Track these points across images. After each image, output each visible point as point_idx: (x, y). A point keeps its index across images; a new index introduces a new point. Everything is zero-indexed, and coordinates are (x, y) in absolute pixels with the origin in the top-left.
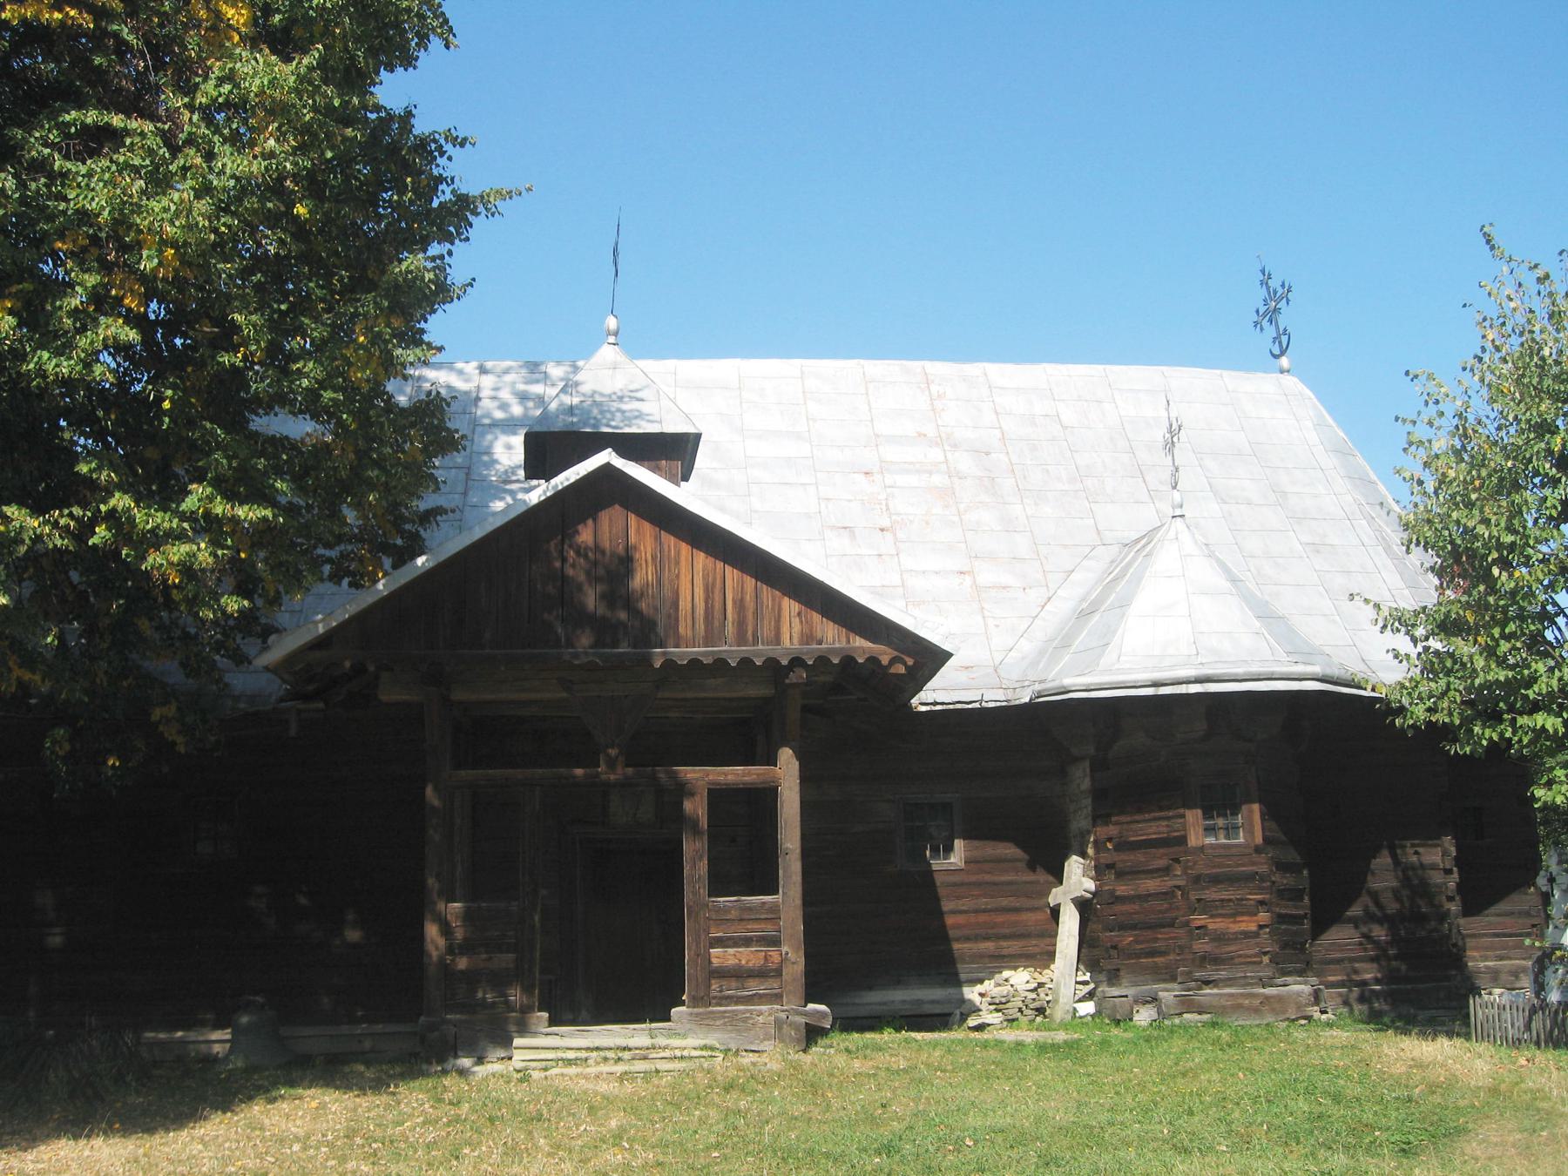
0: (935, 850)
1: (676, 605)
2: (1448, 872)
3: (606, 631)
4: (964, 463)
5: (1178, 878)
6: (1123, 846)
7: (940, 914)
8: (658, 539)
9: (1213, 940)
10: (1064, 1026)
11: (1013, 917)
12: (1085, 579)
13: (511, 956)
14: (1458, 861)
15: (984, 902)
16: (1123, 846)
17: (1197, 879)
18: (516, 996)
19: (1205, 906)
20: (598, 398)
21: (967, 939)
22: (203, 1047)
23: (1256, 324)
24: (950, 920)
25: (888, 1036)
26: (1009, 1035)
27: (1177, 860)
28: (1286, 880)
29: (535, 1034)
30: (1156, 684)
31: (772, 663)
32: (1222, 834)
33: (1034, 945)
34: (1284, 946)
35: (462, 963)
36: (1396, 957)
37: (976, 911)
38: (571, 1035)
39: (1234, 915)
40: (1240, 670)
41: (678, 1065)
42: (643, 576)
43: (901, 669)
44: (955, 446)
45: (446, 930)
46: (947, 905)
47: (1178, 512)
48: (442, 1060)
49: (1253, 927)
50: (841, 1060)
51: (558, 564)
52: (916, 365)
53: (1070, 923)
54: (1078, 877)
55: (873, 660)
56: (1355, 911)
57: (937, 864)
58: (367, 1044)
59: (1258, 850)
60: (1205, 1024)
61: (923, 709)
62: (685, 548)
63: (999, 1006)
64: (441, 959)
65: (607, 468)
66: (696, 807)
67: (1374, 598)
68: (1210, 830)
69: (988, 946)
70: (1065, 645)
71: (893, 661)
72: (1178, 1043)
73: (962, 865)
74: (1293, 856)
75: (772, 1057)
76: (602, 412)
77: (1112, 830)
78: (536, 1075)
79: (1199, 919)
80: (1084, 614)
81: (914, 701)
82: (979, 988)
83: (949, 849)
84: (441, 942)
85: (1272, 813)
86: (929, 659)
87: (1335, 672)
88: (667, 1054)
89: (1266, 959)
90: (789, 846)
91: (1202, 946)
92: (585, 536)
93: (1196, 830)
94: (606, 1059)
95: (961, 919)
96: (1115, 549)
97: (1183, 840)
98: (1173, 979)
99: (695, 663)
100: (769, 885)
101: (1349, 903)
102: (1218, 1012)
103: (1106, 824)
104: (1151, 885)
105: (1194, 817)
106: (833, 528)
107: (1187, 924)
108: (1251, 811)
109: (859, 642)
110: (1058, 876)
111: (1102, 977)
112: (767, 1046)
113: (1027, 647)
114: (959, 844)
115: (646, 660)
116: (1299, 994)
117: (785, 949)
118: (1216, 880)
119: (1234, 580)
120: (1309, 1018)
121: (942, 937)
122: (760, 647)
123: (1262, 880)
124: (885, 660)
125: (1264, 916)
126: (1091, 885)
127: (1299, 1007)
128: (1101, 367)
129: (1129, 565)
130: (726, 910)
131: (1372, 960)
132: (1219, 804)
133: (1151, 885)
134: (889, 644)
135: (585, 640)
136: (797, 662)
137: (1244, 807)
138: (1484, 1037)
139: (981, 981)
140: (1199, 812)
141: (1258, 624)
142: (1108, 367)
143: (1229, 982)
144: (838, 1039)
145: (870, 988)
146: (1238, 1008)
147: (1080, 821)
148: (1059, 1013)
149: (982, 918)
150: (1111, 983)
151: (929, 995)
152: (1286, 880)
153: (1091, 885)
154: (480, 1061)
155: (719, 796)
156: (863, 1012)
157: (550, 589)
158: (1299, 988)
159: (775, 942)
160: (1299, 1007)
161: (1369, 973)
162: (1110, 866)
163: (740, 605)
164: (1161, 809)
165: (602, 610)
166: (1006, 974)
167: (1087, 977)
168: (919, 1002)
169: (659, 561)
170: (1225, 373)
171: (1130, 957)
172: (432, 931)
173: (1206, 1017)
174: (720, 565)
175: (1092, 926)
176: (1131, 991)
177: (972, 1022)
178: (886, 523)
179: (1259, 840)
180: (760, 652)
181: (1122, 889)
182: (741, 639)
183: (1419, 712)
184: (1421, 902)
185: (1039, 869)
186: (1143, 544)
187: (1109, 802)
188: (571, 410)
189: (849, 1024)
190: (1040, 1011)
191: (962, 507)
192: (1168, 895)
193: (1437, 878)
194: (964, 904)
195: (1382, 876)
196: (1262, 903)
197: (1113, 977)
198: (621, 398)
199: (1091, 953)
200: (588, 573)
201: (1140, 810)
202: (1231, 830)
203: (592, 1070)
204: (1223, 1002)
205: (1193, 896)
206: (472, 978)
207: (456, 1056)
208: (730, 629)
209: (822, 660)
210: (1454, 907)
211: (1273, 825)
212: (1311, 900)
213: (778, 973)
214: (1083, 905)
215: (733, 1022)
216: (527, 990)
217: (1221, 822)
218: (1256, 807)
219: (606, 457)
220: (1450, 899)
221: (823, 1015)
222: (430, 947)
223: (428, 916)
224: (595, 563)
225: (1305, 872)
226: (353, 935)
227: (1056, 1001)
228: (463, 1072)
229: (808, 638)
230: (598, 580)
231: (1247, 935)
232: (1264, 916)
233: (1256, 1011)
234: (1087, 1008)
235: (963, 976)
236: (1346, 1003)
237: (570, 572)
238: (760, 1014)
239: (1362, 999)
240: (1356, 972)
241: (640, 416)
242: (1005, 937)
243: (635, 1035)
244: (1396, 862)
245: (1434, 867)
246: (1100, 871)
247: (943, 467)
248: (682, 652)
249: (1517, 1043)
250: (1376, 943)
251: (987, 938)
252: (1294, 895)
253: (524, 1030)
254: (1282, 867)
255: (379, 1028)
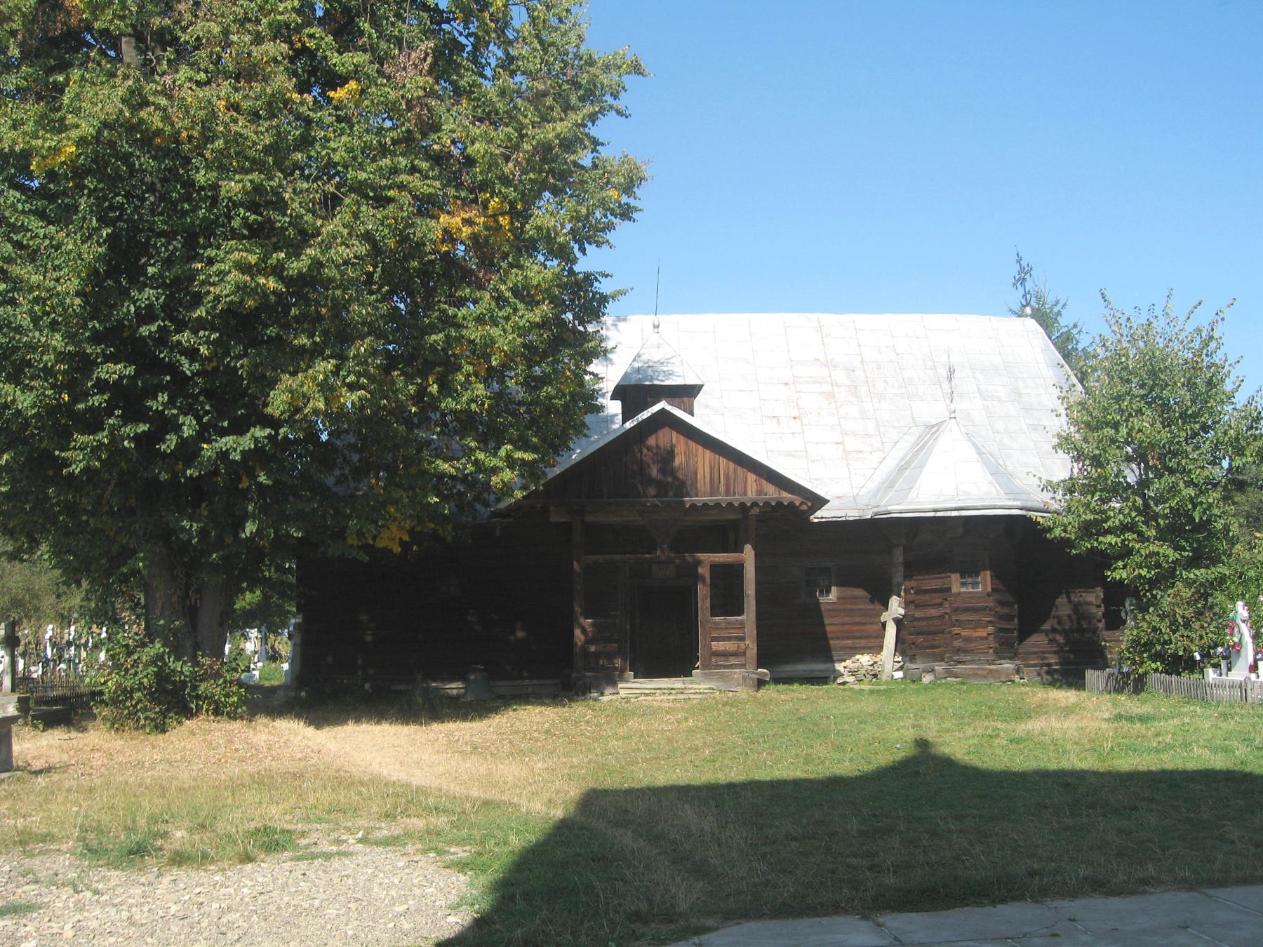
0: (821, 592)
1: (696, 473)
2: (1099, 606)
3: (662, 488)
4: (839, 376)
5: (946, 609)
6: (919, 592)
7: (823, 625)
8: (687, 444)
9: (963, 640)
10: (886, 683)
11: (862, 628)
12: (905, 446)
13: (616, 645)
14: (1104, 601)
15: (847, 619)
16: (919, 592)
17: (956, 609)
18: (618, 663)
19: (959, 623)
20: (651, 364)
21: (838, 638)
22: (443, 692)
23: (1014, 284)
24: (828, 629)
25: (796, 686)
26: (857, 687)
27: (946, 600)
28: (1005, 610)
29: (627, 681)
30: (935, 511)
31: (743, 505)
32: (970, 586)
33: (873, 642)
34: (1002, 644)
35: (593, 648)
36: (1068, 652)
37: (843, 624)
38: (645, 683)
39: (974, 628)
40: (978, 504)
41: (697, 696)
42: (679, 460)
43: (805, 508)
44: (835, 367)
45: (584, 631)
46: (827, 621)
47: (953, 416)
48: (584, 694)
49: (985, 634)
50: (775, 695)
51: (639, 455)
52: (813, 316)
53: (891, 631)
54: (896, 607)
55: (791, 504)
56: (1046, 626)
57: (822, 599)
58: (530, 690)
59: (988, 595)
60: (958, 683)
61: (816, 520)
62: (700, 448)
63: (853, 673)
64: (583, 647)
65: (663, 411)
66: (704, 571)
67: (1038, 475)
68: (963, 584)
69: (849, 642)
70: (891, 486)
71: (802, 503)
72: (940, 690)
73: (835, 600)
74: (1008, 597)
75: (743, 693)
76: (654, 372)
77: (913, 583)
78: (632, 700)
79: (956, 630)
80: (902, 469)
81: (812, 517)
82: (843, 664)
83: (829, 591)
84: (582, 637)
85: (997, 576)
86: (820, 502)
87: (1029, 504)
88: (692, 691)
89: (991, 651)
90: (749, 592)
91: (958, 644)
92: (651, 441)
93: (956, 583)
94: (664, 694)
95: (834, 628)
96: (921, 429)
97: (949, 589)
98: (942, 660)
99: (705, 505)
100: (740, 612)
101: (1044, 621)
102: (965, 677)
103: (910, 580)
104: (933, 612)
105: (955, 577)
106: (768, 417)
107: (950, 632)
108: (985, 575)
109: (785, 494)
110: (886, 606)
111: (907, 659)
112: (739, 689)
113: (871, 486)
114: (834, 589)
115: (683, 503)
116: (1007, 669)
117: (747, 642)
118: (967, 610)
119: (980, 454)
120: (1013, 681)
121: (824, 637)
122: (737, 497)
123: (990, 610)
124: (797, 504)
125: (991, 629)
126: (902, 611)
127: (1007, 675)
128: (919, 316)
129: (927, 442)
130: (718, 623)
131: (1055, 652)
132: (969, 570)
133: (933, 612)
134: (799, 495)
135: (652, 491)
136: (755, 504)
137: (982, 573)
138: (1091, 690)
139: (845, 661)
140: (958, 575)
141: (990, 478)
142: (924, 315)
143: (972, 662)
144: (772, 687)
145: (787, 663)
146: (975, 675)
147: (898, 578)
148: (884, 677)
149: (846, 628)
150: (911, 662)
151: (818, 667)
152: (1005, 610)
153: (902, 611)
154: (602, 694)
155: (715, 567)
156: (782, 676)
157: (636, 467)
158: (1008, 666)
159: (742, 639)
160: (1007, 675)
161: (1053, 659)
162: (912, 602)
163: (727, 477)
164: (938, 573)
165: (660, 477)
166: (858, 657)
167: (900, 659)
168: (812, 671)
169: (688, 455)
170: (993, 318)
171: (921, 648)
172: (578, 632)
173: (958, 679)
174: (717, 456)
175: (903, 632)
176: (921, 666)
177: (839, 681)
178: (796, 413)
179: (989, 589)
180: (736, 499)
181: (918, 614)
182: (727, 493)
183: (1057, 532)
184: (1083, 622)
185: (876, 603)
186: (933, 430)
187: (911, 569)
188: (638, 370)
189: (777, 681)
190: (875, 676)
191: (838, 404)
192: (941, 617)
193: (1093, 610)
194: (838, 620)
195: (1063, 607)
196: (990, 622)
197: (913, 659)
198: (662, 363)
199: (902, 646)
200: (653, 459)
201: (928, 573)
202: (975, 584)
203: (659, 698)
204: (968, 672)
205: (954, 618)
206: (597, 655)
207: (590, 692)
208: (722, 488)
209: (767, 503)
210: (1101, 625)
211: (998, 582)
212: (1019, 621)
213: (744, 654)
214: (898, 622)
215: (722, 677)
216: (624, 660)
217: (970, 580)
218: (988, 573)
219: (662, 405)
220: (1100, 621)
221: (766, 674)
222: (577, 640)
223: (576, 626)
224: (656, 454)
225: (1016, 606)
226: (520, 634)
227: (883, 671)
228: (596, 700)
229: (760, 492)
230: (658, 462)
231: (981, 638)
232: (991, 629)
233: (984, 677)
234: (899, 675)
235: (835, 658)
236: (1039, 674)
237: (644, 459)
238: (735, 673)
239: (1048, 673)
240: (1045, 658)
241: (671, 374)
242: (858, 638)
243: (677, 683)
244: (1070, 601)
245: (1090, 604)
246: (907, 604)
247: (828, 380)
248: (700, 500)
249: (1101, 693)
250: (1059, 644)
251: (848, 638)
252: (1009, 618)
253: (622, 679)
254: (1001, 603)
255: (535, 681)
